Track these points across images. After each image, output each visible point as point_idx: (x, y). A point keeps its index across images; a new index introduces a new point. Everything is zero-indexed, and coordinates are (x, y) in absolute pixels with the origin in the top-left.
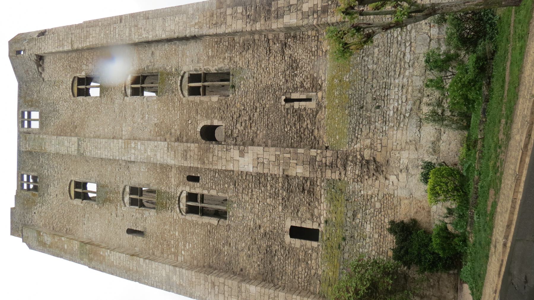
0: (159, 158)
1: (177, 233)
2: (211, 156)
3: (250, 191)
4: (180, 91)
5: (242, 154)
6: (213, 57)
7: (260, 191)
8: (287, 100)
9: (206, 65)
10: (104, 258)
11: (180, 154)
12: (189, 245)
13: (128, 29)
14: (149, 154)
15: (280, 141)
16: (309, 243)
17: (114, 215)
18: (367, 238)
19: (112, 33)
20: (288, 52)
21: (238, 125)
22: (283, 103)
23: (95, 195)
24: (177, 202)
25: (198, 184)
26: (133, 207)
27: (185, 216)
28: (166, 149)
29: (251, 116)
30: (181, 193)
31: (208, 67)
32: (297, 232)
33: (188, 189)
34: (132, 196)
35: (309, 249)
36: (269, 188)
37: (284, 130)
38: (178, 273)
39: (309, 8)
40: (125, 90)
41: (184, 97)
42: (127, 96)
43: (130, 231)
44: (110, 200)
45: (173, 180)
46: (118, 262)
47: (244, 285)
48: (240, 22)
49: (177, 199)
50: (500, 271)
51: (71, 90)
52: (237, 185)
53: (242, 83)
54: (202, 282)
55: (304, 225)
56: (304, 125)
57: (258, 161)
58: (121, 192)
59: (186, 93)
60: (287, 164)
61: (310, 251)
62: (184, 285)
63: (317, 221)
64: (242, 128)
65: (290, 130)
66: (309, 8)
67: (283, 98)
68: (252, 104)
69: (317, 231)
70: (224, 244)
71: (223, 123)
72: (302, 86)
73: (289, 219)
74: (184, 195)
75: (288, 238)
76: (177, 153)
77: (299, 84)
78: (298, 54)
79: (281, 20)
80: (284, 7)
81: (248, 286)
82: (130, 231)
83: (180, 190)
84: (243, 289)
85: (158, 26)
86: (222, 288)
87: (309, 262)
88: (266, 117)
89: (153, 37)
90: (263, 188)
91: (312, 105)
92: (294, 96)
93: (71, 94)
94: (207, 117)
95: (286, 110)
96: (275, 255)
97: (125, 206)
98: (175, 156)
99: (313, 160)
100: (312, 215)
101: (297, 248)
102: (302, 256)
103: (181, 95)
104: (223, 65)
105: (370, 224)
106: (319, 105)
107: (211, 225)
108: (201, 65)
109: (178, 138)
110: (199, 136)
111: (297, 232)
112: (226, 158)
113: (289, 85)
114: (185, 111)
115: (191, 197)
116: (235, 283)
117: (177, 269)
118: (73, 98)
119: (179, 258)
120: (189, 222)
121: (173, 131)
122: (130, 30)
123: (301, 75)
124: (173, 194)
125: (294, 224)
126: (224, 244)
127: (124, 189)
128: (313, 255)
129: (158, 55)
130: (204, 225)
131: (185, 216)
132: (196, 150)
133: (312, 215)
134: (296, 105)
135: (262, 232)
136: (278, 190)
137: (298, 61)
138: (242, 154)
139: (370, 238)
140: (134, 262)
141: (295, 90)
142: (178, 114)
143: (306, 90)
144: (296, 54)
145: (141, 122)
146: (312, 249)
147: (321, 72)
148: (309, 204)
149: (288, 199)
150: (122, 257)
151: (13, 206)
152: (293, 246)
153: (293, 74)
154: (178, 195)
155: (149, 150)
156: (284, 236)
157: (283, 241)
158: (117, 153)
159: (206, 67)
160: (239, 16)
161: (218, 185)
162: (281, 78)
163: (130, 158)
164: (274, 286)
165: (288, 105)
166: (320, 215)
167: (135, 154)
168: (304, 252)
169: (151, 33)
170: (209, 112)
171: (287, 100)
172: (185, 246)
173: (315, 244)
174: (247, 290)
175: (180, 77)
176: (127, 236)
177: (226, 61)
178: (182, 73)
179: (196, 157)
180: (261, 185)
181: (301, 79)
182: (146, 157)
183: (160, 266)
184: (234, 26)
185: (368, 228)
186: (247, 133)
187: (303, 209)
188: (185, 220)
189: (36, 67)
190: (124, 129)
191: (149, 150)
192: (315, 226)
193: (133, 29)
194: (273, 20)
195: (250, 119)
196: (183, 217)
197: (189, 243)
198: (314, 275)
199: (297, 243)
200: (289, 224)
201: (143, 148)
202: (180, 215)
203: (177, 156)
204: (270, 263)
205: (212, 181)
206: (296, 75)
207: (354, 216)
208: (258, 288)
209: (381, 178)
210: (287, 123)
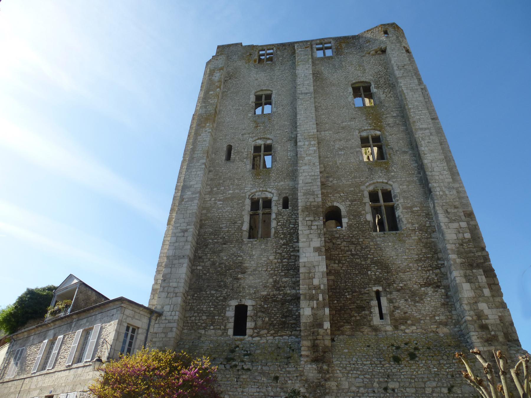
0: (303, 168)
1: (231, 192)
2: (312, 218)
3: (279, 260)
4: (372, 182)
5: (317, 250)
6: (412, 212)
7: (280, 271)
9: (402, 205)
11: (309, 188)
12: (220, 204)
13: (426, 126)
14: (306, 158)
15: (334, 289)
16: (231, 326)
17: (244, 132)
18: (241, 389)
19: (420, 112)
22: (375, 289)
24: (261, 189)
25: (281, 208)
26: (253, 148)
27: (249, 198)
28: (313, 174)
29: (356, 257)
30: (271, 193)
31: (401, 207)
32: (241, 310)
33: (275, 198)
35: (225, 326)
37: (346, 292)
38: (194, 196)
39: (482, 311)
40: (365, 130)
43: (230, 149)
44: (257, 127)
45: (282, 183)
46: (201, 140)
49: (264, 189)
51: (357, 81)
52: (283, 247)
53: (390, 244)
57: (311, 268)
59: (371, 188)
60: (312, 298)
61: (222, 327)
62: (183, 203)
63: (254, 332)
64: (342, 248)
65: (347, 298)
66: (482, 311)
67: (380, 289)
68: (369, 256)
69: (244, 334)
70: (224, 237)
71: (345, 228)
73: (254, 303)
74: (269, 196)
75: (234, 303)
76: (310, 184)
77: (396, 304)
78: (430, 301)
79: (464, 280)
80: (479, 282)
81: (185, 265)
82: (230, 149)
83: (273, 191)
85: (435, 154)
87: (212, 327)
88: (357, 272)
89: (423, 151)
90: (283, 274)
91: (376, 320)
92: (384, 301)
93: (354, 81)
94: (349, 212)
95: (367, 292)
96: (216, 290)
98: (307, 183)
99: (321, 326)
101: (225, 313)
102: (218, 319)
103: (367, 184)
104: (405, 222)
105: (257, 392)
106: (376, 329)
107: (242, 224)
109: (325, 184)
111: (241, 310)
112: (310, 233)
114: (352, 189)
115: (268, 203)
117: (197, 195)
118: (350, 83)
119: (207, 196)
120: (244, 202)
121: (331, 179)
122: (426, 129)
123: (407, 306)
124: (269, 184)
125: (249, 308)
126: (224, 237)
128: (219, 331)
129: (405, 158)
130: (242, 217)
131: (249, 198)
134: (374, 303)
135: (239, 276)
136: (283, 290)
137: (422, 302)
138: (317, 250)
139: (243, 392)
140: (201, 155)
141: (390, 301)
142: (348, 183)
143: (392, 314)
144: (429, 299)
145: (336, 148)
146: (226, 330)
147: (415, 328)
148: (271, 324)
149: (275, 301)
150: (205, 143)
152: (228, 309)
153: (407, 297)
154: (268, 190)
155: (309, 158)
156: (236, 299)
157: (232, 298)
159: (400, 205)
160: (461, 236)
161: (281, 228)
162: (401, 285)
163: (300, 141)
165: (373, 294)
167: (304, 145)
168: (221, 321)
170: (355, 215)
171: (378, 293)
172: (220, 200)
173: (231, 332)
175: (385, 181)
177: (409, 226)
178: (390, 182)
179: (308, 204)
180: (286, 271)
181: (402, 307)
182: (303, 156)
184: (449, 231)
186: (337, 253)
188: (244, 198)
189: (376, 48)
191: (309, 158)
193: (427, 131)
194: (462, 272)
196: (247, 196)
197: (222, 204)
198: (199, 333)
199: (230, 313)
200: (249, 302)
202: (249, 193)
203: (306, 185)
204: (208, 286)
205: (285, 221)
206: (406, 300)
208: (184, 276)
210: (354, 294)
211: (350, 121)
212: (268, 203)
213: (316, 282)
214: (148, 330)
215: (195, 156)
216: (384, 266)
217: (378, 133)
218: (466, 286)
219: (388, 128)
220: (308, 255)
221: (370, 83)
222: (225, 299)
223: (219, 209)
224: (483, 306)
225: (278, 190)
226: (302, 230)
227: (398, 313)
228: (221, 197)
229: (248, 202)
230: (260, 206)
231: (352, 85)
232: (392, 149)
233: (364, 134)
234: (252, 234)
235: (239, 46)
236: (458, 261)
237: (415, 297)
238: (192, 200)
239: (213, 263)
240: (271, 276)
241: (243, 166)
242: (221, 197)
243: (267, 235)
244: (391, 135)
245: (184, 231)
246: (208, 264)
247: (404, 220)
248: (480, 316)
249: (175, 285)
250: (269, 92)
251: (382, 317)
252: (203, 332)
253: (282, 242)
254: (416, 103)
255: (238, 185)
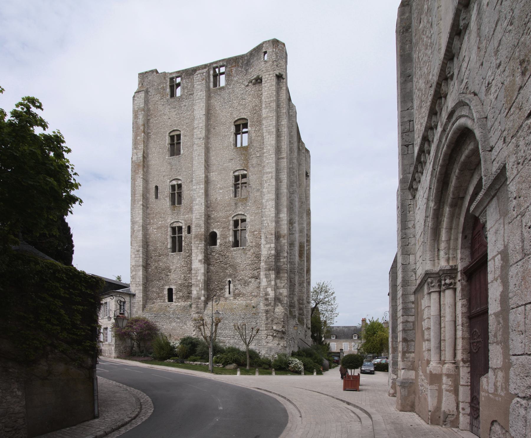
2: (198, 242)
5: (200, 261)
8: (230, 282)
10: (138, 173)
14: (198, 199)
16: (166, 298)
20: (253, 279)
21: (217, 255)
22: (228, 280)
23: (217, 72)
32: (170, 291)
34: (176, 186)
36: (188, 275)
41: (233, 218)
42: (234, 172)
43: (157, 187)
44: (171, 169)
45: (187, 216)
47: (141, 268)
48: (266, 253)
50: (261, 389)
51: (239, 118)
54: (138, 244)
55: (174, 295)
56: (218, 292)
58: (177, 178)
59: (235, 219)
60: (197, 286)
67: (231, 280)
69: (172, 301)
72: (236, 289)
73: (175, 287)
74: (181, 225)
75: (167, 287)
79: (264, 277)
81: (141, 270)
82: (157, 187)
84: (139, 268)
85: (270, 195)
86: (138, 256)
91: (227, 295)
92: (231, 285)
93: (236, 119)
94: (221, 235)
97: (170, 182)
99: (200, 298)
100: (179, 298)
106: (226, 299)
107: (167, 244)
108: (249, 227)
110: (212, 230)
111: (170, 291)
113: (237, 282)
116: (141, 263)
120: (167, 230)
125: (174, 290)
127: (179, 180)
130: (167, 239)
132: (200, 233)
133: (179, 298)
134: (227, 287)
138: (200, 261)
141: (234, 286)
143: (234, 292)
146: (164, 300)
151: (159, 72)
158: (197, 174)
160: (269, 252)
164: (146, 283)
165: (227, 282)
166: (179, 302)
169: (266, 190)
170: (225, 237)
171: (230, 282)
172: (155, 229)
173: (167, 300)
174: (139, 270)
175: (243, 213)
176: (154, 187)
177: (251, 244)
178: (246, 214)
183: (141, 216)
184: (265, 249)
185: (174, 324)
187: (181, 294)
190: (214, 173)
192: (174, 300)
193: (270, 175)
194: (264, 272)
195: (221, 262)
199: (166, 292)
200: (173, 287)
201: (200, 194)
207: (178, 318)
208: (141, 276)
209: (194, 329)
211: (229, 162)
212: (180, 228)
213: (199, 278)
214: (130, 302)
215: (136, 198)
216: (234, 267)
217: (245, 172)
218: (264, 280)
219: (251, 169)
220: (196, 264)
221: (247, 120)
222: (163, 286)
223: (155, 235)
224: (269, 290)
225: (185, 221)
226: (194, 250)
227: (237, 291)
228: (155, 226)
229: (169, 229)
230: (176, 231)
231: (235, 122)
232: (251, 187)
233: (236, 174)
234: (174, 250)
235: (155, 73)
236: (265, 266)
237: (246, 283)
238: (138, 231)
239: (156, 268)
240: (183, 273)
241: (165, 202)
242: (155, 226)
243: (180, 250)
244: (252, 175)
245: (138, 251)
246: (153, 267)
247: (248, 240)
248: (267, 294)
249: (138, 280)
250: (178, 133)
251: (229, 294)
252: (155, 301)
253: (187, 254)
254: (269, 147)
255: (164, 218)
